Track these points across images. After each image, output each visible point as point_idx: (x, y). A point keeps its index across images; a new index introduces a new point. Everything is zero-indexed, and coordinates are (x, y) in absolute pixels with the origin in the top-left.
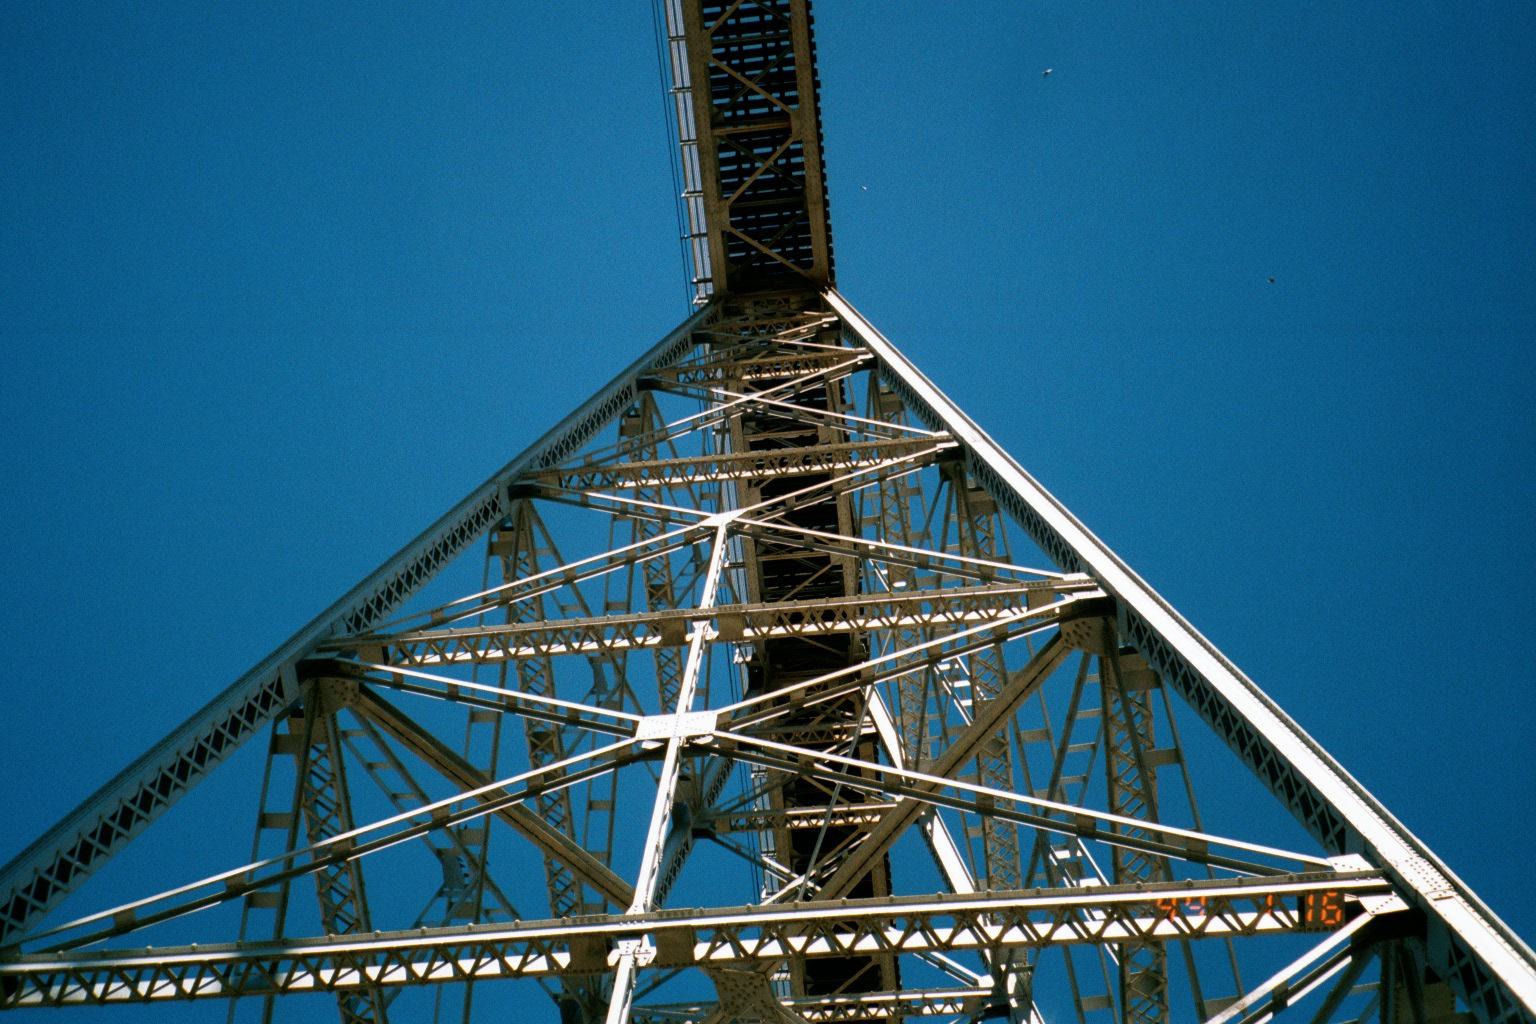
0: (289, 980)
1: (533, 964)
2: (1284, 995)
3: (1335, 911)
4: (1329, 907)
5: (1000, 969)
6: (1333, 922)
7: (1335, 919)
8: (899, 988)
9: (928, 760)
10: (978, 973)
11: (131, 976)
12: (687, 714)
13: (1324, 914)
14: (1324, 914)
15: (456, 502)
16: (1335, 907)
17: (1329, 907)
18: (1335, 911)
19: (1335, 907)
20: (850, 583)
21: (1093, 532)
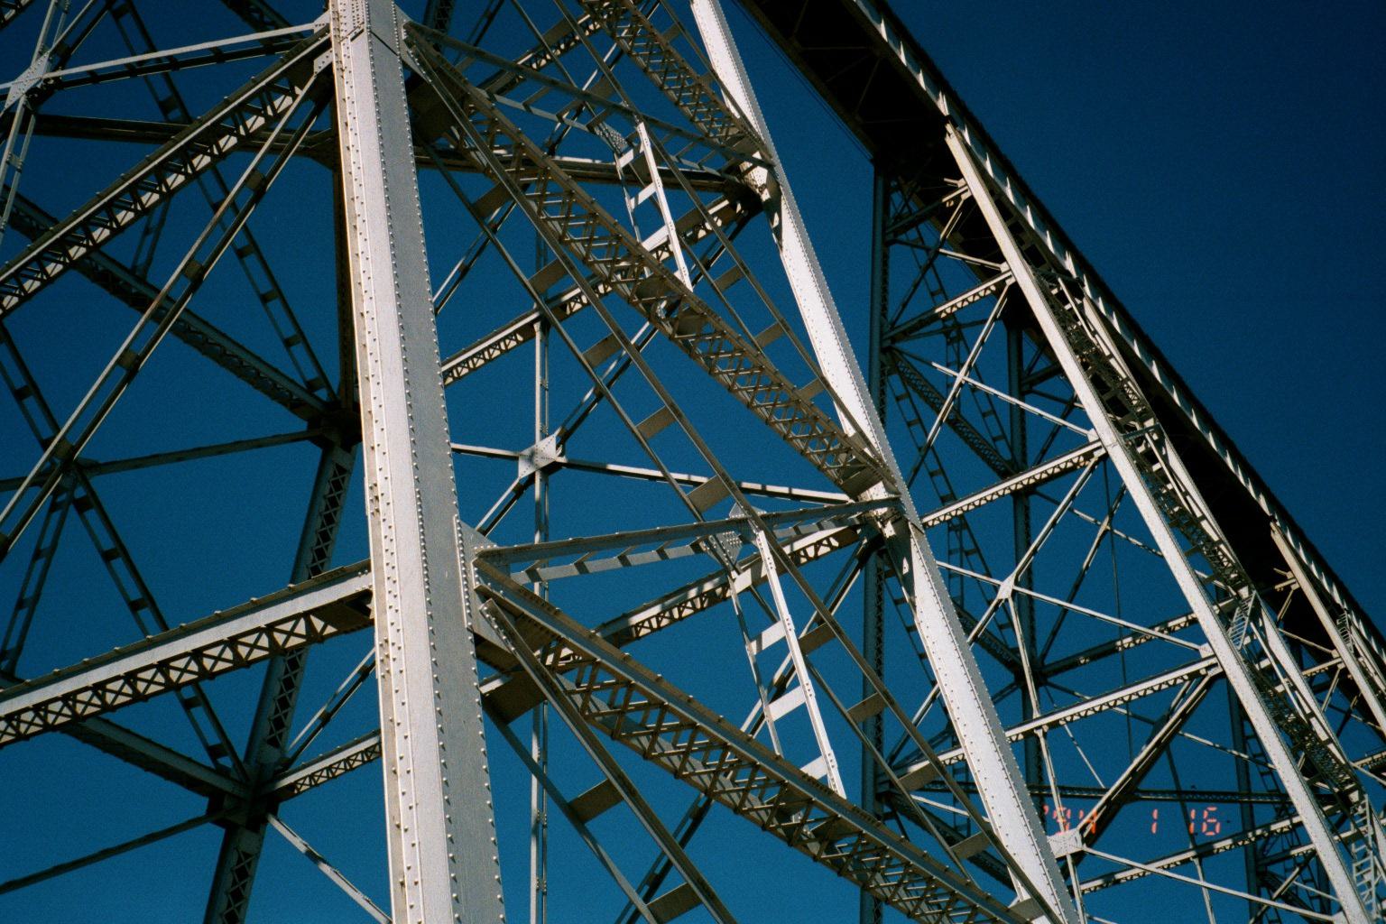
0: (571, 309)
1: (846, 560)
2: (263, 183)
3: (1215, 824)
4: (1209, 821)
5: (755, 152)
6: (1213, 834)
7: (1207, 831)
8: (158, 291)
9: (186, 317)
10: (954, 179)
11: (255, 105)
12: (741, 575)
13: (1205, 827)
14: (1205, 827)
15: (320, 361)
16: (1214, 821)
17: (1209, 821)
18: (1215, 824)
19: (1214, 821)
20: (150, 294)
21: (1084, 754)
